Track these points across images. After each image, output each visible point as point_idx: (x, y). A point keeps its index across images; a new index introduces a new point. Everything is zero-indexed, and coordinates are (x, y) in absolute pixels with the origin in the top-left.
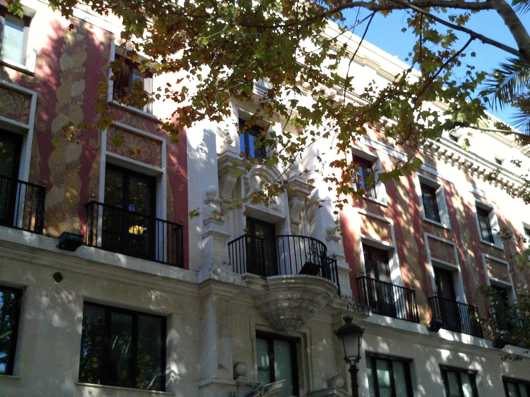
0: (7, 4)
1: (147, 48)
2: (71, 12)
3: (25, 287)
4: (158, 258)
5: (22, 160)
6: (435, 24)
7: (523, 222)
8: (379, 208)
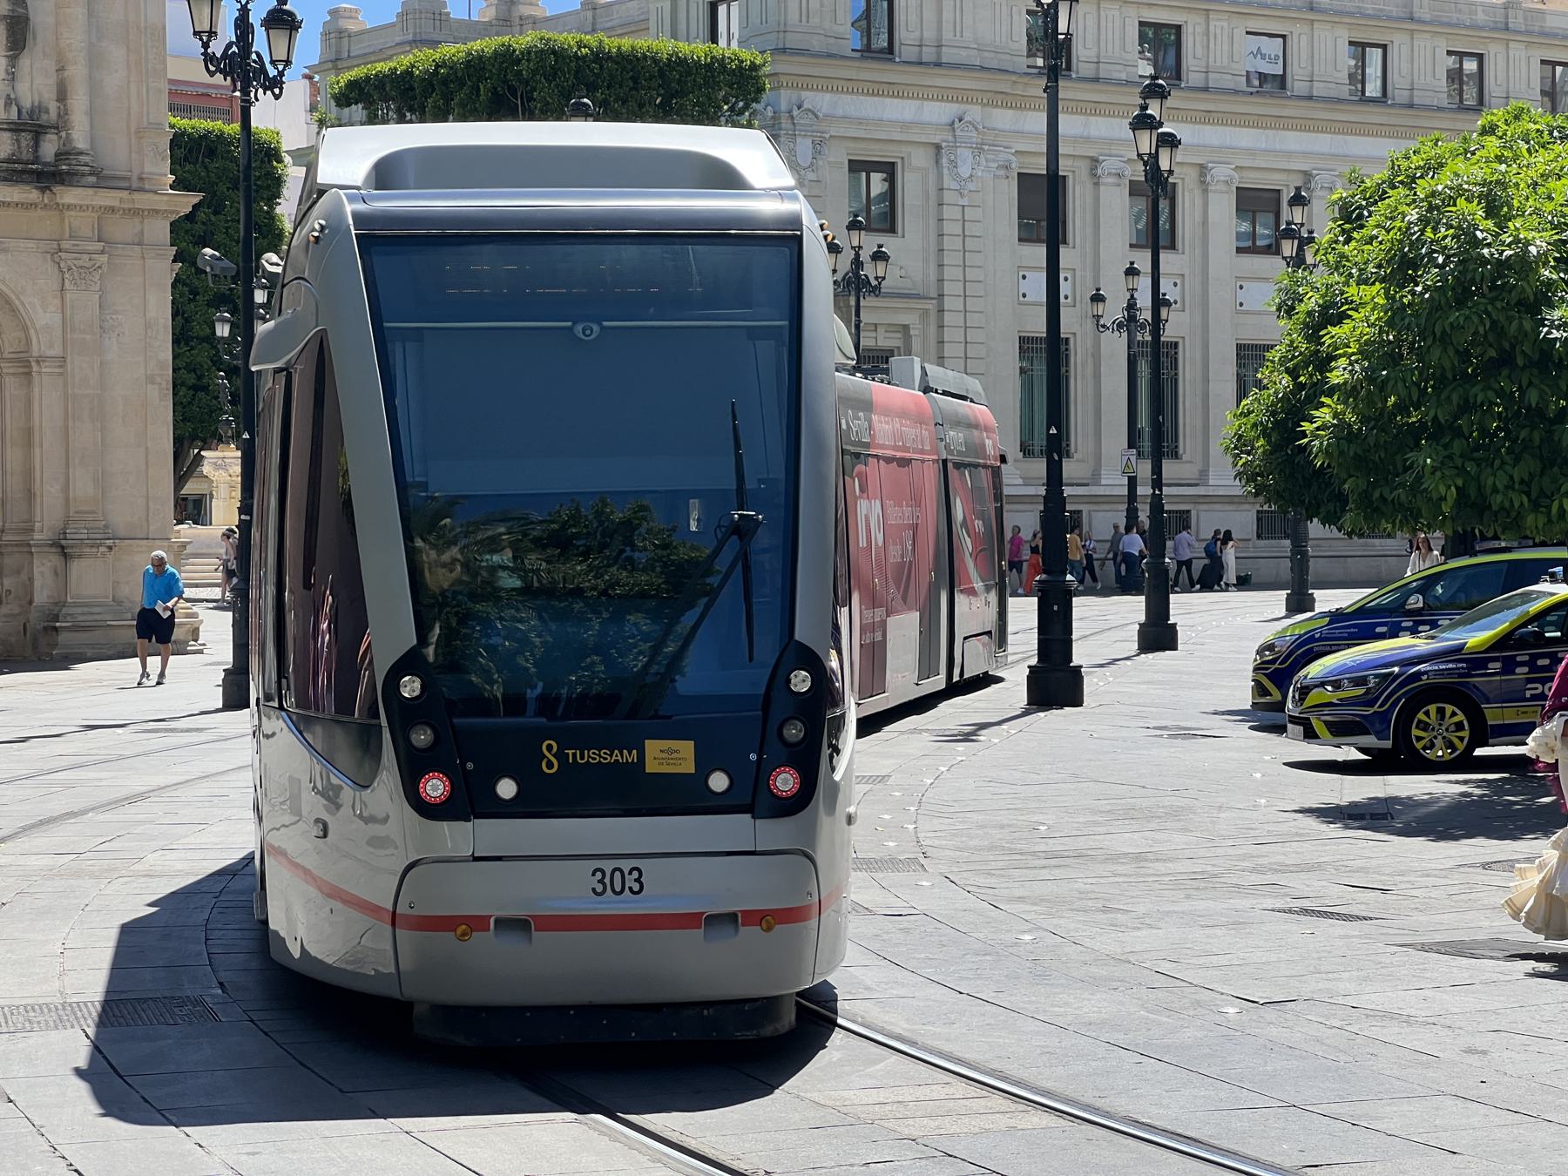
0: (1276, 601)
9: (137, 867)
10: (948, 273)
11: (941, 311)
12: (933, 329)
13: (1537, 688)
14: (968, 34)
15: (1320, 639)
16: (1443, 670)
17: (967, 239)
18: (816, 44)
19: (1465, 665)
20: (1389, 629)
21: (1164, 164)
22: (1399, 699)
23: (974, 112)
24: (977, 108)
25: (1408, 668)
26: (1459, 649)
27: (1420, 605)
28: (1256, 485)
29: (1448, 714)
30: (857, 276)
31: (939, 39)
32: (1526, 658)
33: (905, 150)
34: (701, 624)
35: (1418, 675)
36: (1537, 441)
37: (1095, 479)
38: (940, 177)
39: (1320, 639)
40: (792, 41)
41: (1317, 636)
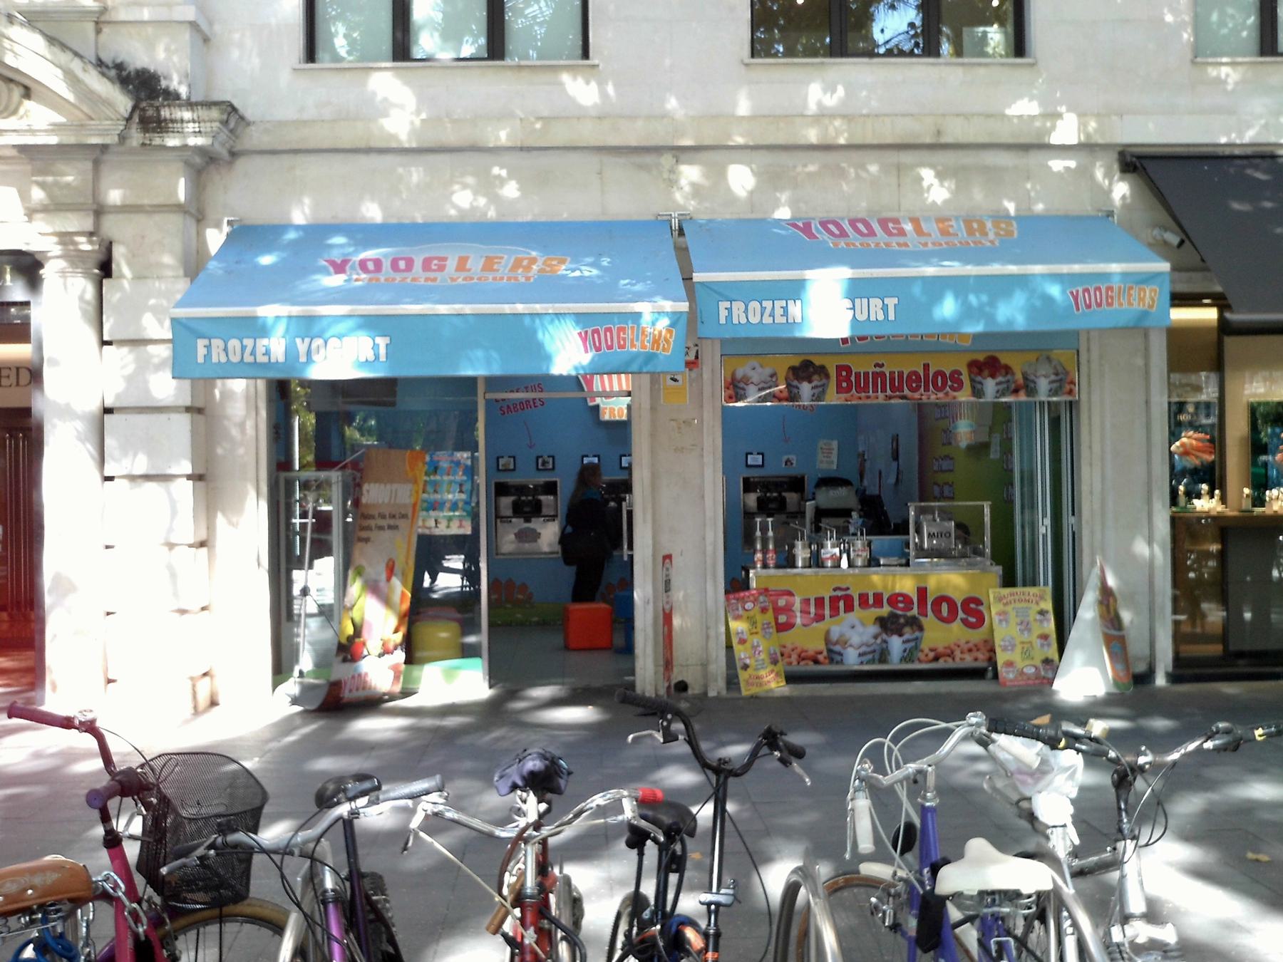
3: (759, 49)
4: (173, 503)
7: (274, 689)
9: (317, 919)
17: (254, 381)
34: (665, 647)
36: (538, 20)
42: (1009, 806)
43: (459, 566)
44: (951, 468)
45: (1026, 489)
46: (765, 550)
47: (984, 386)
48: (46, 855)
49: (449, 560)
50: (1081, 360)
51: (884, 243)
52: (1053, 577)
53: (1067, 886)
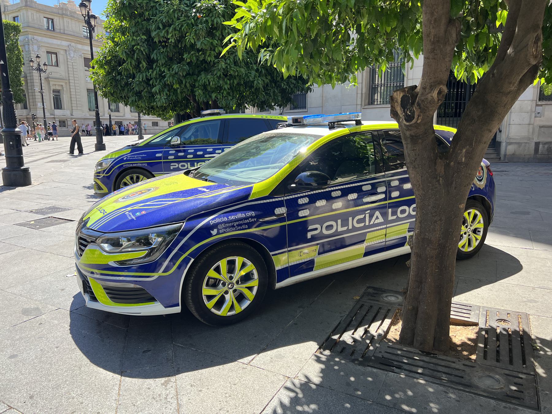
0: (136, 137)
1: (342, 226)
2: (397, 91)
5: (323, 274)
6: (89, 188)
8: (171, 136)
10: (70, 75)
11: (69, 83)
12: (68, 86)
13: (316, 229)
14: (70, 28)
15: (127, 160)
16: (232, 221)
18: (36, 26)
19: (253, 213)
20: (163, 154)
21: (93, 23)
22: (186, 261)
23: (73, 44)
24: (74, 44)
25: (193, 222)
26: (245, 196)
27: (179, 142)
28: (103, 92)
29: (249, 284)
30: (40, 68)
31: (64, 28)
32: (193, 151)
33: (59, 50)
35: (206, 231)
37: (104, 115)
38: (67, 57)
39: (127, 160)
40: (30, 25)
41: (125, 159)
42: (545, 4)
43: (390, 336)
44: (488, 358)
45: (513, 401)
46: (232, 225)
47: (141, 237)
48: (431, 388)
49: (394, 339)
50: (77, 35)
51: (409, 231)
52: (352, 211)
53: (153, 276)
